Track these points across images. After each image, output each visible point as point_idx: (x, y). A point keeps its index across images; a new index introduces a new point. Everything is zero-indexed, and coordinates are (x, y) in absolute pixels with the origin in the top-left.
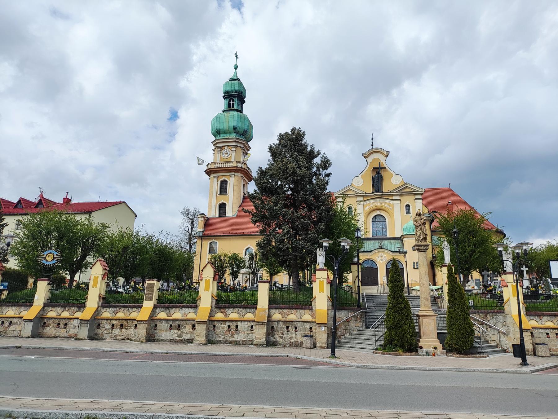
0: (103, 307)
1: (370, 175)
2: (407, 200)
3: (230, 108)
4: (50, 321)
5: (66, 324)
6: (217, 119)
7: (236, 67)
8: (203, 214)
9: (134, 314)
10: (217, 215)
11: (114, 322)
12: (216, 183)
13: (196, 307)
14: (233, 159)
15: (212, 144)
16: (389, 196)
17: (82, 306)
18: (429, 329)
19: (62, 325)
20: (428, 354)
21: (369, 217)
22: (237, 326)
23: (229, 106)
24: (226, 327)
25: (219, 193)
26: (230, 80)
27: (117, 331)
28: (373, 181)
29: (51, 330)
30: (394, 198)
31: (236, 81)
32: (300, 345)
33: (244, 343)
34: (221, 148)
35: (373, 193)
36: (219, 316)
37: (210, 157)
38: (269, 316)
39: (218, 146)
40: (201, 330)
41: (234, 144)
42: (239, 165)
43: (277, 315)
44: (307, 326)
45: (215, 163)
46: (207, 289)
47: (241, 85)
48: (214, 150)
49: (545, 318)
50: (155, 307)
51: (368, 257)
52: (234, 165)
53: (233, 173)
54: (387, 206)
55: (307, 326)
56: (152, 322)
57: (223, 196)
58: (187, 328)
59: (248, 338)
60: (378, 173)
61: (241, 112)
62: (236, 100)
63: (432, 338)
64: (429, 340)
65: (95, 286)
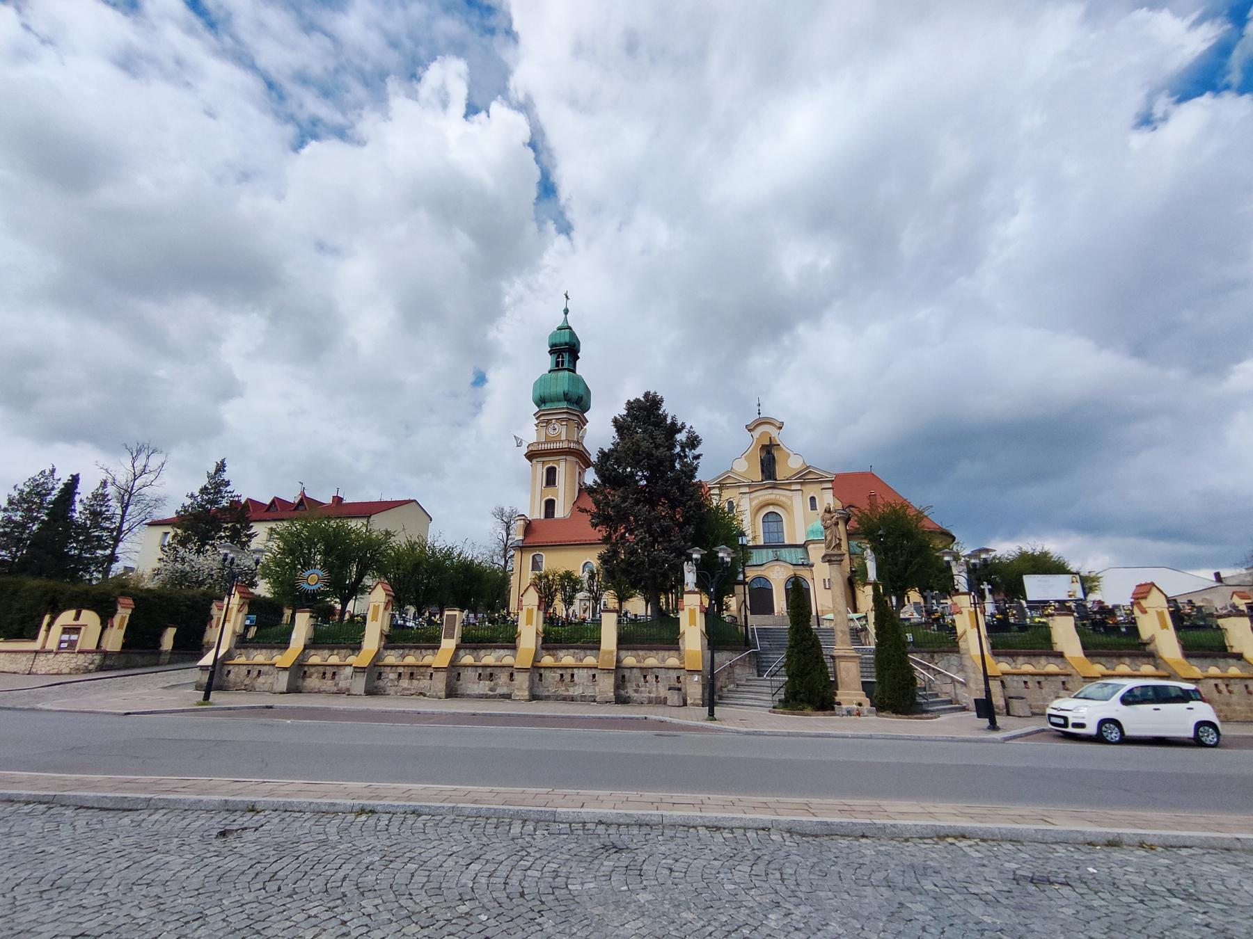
0: (386, 648)
2: (812, 490)
3: (558, 366)
4: (312, 670)
5: (334, 674)
6: (541, 382)
7: (566, 311)
9: (429, 658)
11: (401, 670)
12: (541, 471)
13: (515, 648)
16: (785, 486)
17: (356, 647)
18: (850, 676)
19: (329, 675)
20: (849, 713)
22: (572, 675)
23: (557, 364)
24: (558, 676)
27: (405, 683)
29: (313, 682)
30: (793, 487)
32: (663, 702)
33: (583, 699)
36: (547, 660)
37: (531, 434)
38: (619, 661)
39: (543, 420)
40: (522, 680)
42: (572, 445)
43: (629, 660)
44: (673, 674)
46: (529, 622)
47: (573, 334)
50: (458, 648)
52: (565, 445)
54: (783, 499)
55: (673, 674)
56: (454, 669)
58: (503, 678)
59: (589, 692)
60: (769, 452)
62: (566, 356)
64: (850, 694)
65: (375, 619)
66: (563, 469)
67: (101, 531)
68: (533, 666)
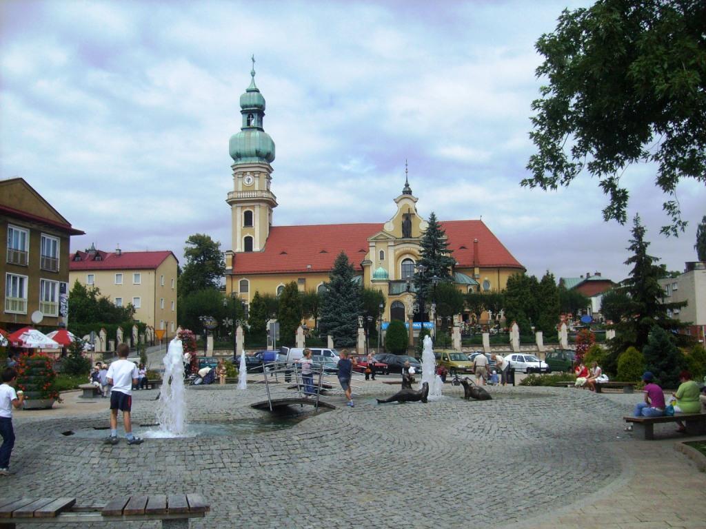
1: (401, 220)
3: (248, 127)
6: (233, 141)
7: (253, 74)
8: (231, 251)
10: (243, 251)
14: (257, 188)
25: (243, 225)
26: (248, 91)
28: (403, 227)
31: (256, 93)
34: (243, 174)
35: (403, 238)
39: (239, 172)
48: (234, 175)
51: (397, 299)
52: (259, 194)
53: (257, 204)
57: (248, 229)
61: (261, 130)
67: (575, 147)
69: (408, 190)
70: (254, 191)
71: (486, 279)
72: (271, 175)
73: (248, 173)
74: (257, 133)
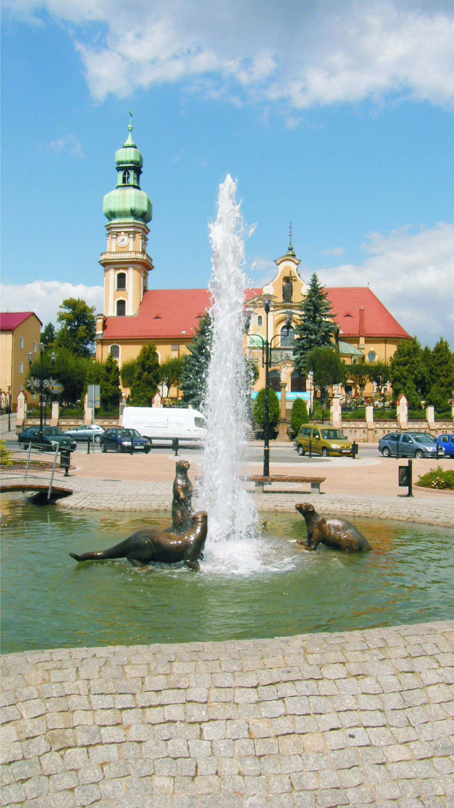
0: (27, 418)
10: (115, 314)
15: (105, 229)
21: (279, 326)
41: (132, 230)
42: (140, 256)
45: (136, 252)
49: (352, 423)
52: (133, 256)
62: (132, 173)
63: (285, 441)
65: (21, 407)
66: (131, 275)
68: (23, 425)
69: (291, 253)
70: (131, 252)
71: (372, 349)
72: (148, 236)
73: (123, 233)
74: (133, 191)
